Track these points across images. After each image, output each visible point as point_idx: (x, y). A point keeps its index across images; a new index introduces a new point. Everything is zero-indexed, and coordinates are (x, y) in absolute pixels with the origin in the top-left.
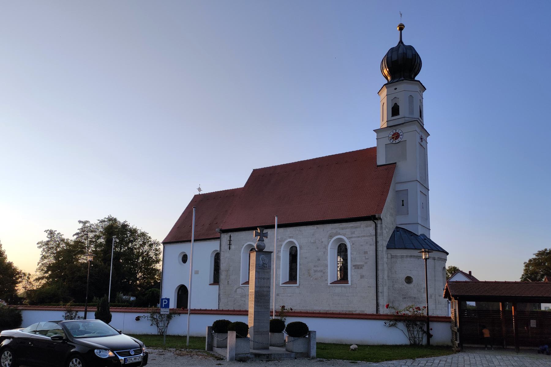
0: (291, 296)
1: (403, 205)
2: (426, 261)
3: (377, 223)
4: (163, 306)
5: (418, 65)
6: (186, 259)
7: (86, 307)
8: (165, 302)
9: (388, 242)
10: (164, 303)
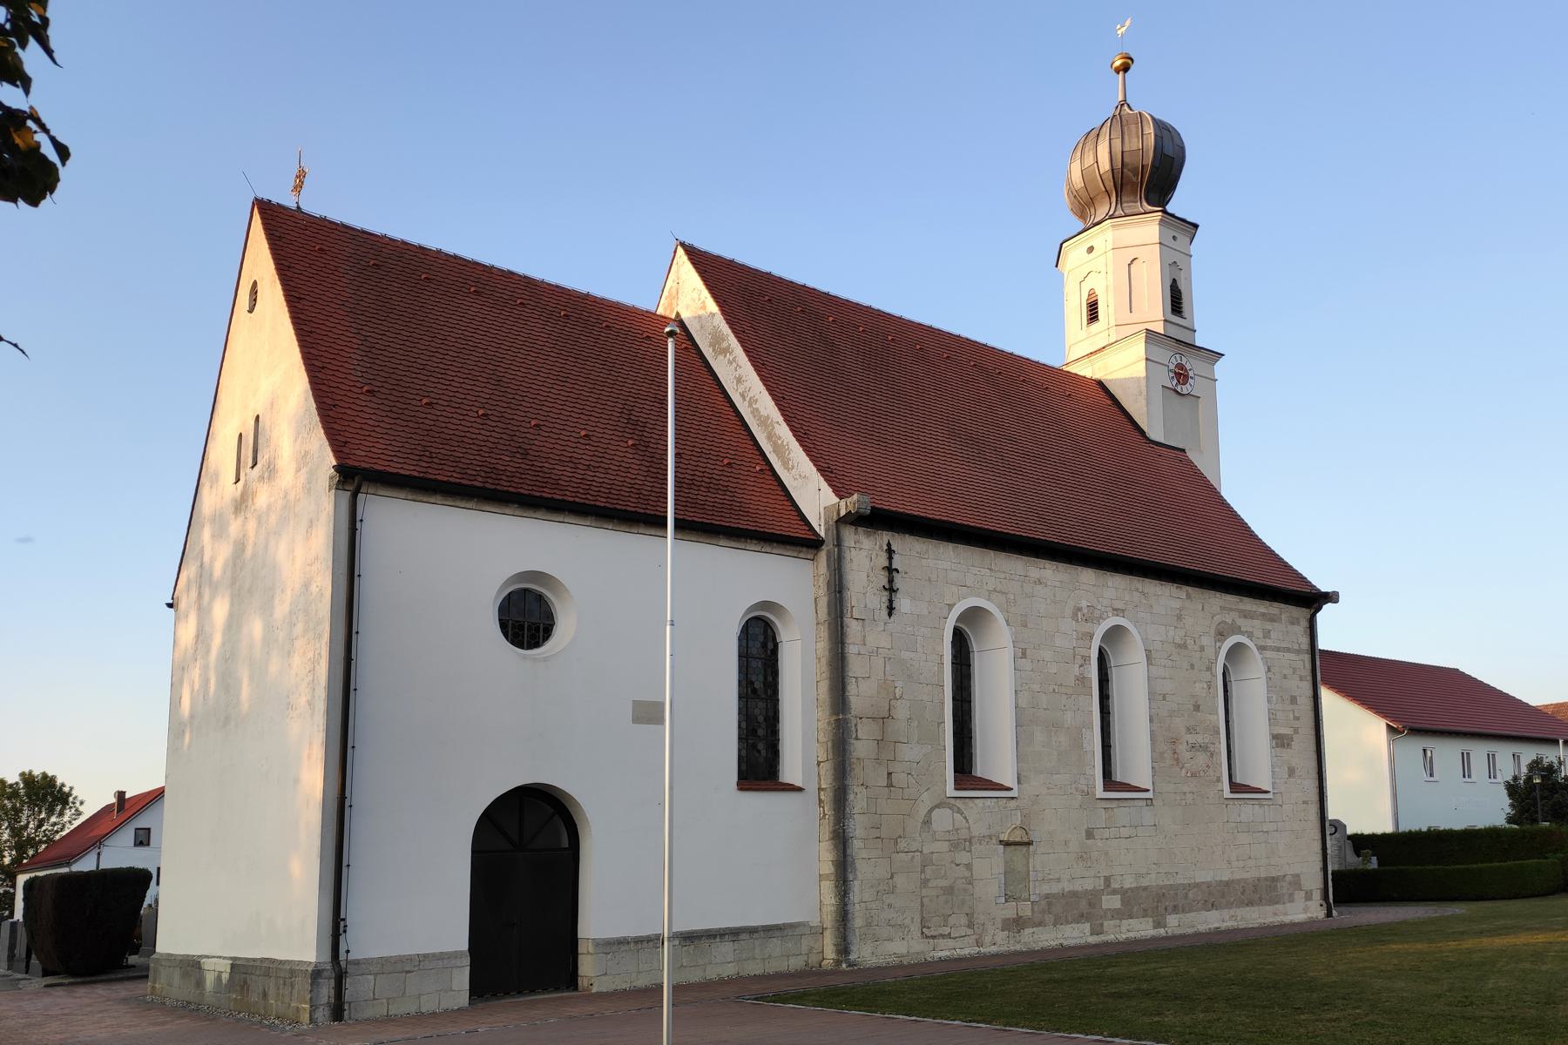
0: (1130, 837)
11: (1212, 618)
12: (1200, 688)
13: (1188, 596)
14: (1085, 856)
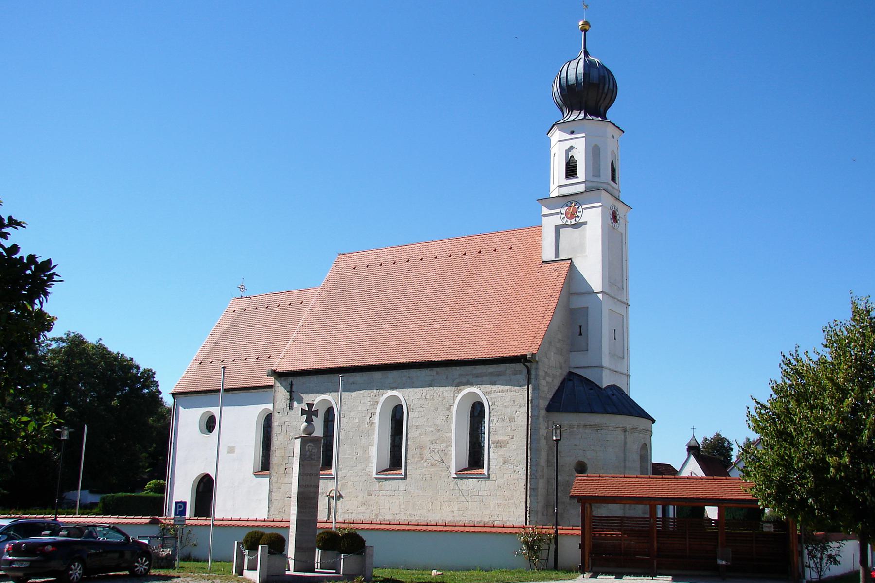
0: (390, 496)
1: (581, 334)
2: (557, 444)
3: (529, 367)
4: (178, 513)
5: (609, 96)
6: (214, 424)
7: (56, 516)
8: (180, 507)
9: (549, 400)
10: (178, 509)
11: (453, 381)
12: (440, 420)
13: (437, 373)
14: (366, 503)
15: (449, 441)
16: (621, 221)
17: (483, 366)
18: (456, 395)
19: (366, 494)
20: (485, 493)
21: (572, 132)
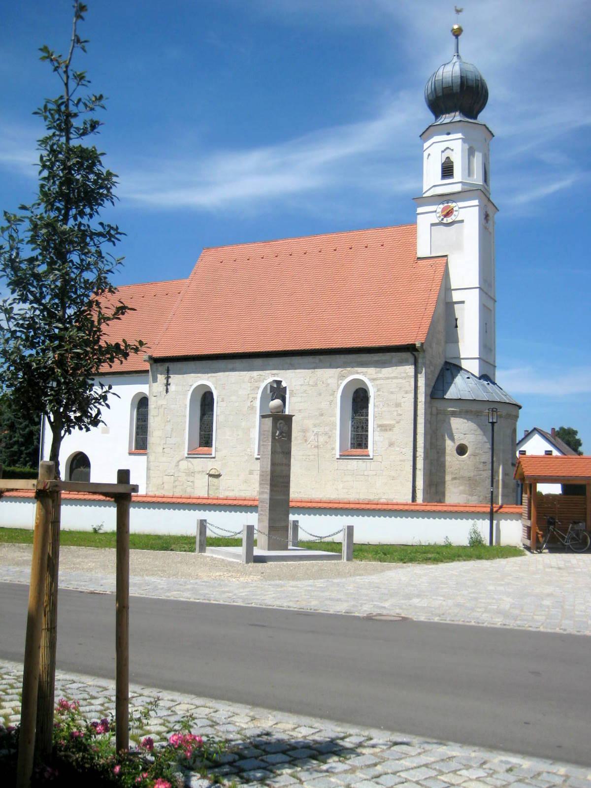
15: (334, 425)
16: (490, 222)
17: (368, 355)
18: (340, 381)
19: (248, 473)
20: (371, 473)
21: (448, 134)
